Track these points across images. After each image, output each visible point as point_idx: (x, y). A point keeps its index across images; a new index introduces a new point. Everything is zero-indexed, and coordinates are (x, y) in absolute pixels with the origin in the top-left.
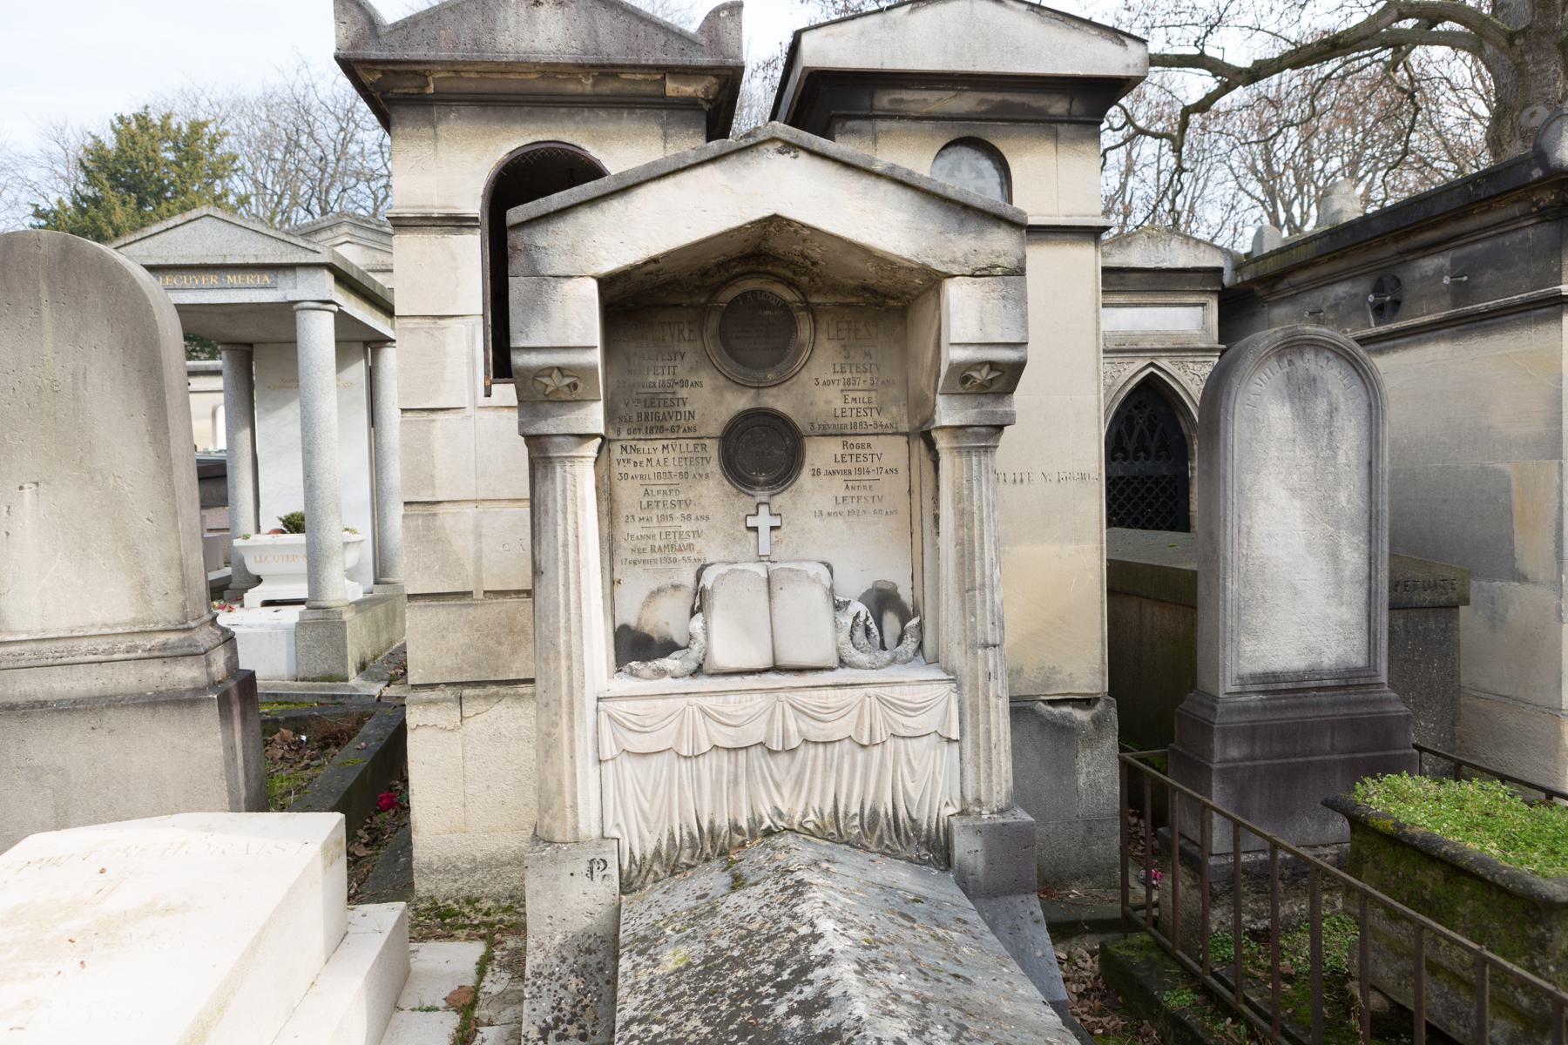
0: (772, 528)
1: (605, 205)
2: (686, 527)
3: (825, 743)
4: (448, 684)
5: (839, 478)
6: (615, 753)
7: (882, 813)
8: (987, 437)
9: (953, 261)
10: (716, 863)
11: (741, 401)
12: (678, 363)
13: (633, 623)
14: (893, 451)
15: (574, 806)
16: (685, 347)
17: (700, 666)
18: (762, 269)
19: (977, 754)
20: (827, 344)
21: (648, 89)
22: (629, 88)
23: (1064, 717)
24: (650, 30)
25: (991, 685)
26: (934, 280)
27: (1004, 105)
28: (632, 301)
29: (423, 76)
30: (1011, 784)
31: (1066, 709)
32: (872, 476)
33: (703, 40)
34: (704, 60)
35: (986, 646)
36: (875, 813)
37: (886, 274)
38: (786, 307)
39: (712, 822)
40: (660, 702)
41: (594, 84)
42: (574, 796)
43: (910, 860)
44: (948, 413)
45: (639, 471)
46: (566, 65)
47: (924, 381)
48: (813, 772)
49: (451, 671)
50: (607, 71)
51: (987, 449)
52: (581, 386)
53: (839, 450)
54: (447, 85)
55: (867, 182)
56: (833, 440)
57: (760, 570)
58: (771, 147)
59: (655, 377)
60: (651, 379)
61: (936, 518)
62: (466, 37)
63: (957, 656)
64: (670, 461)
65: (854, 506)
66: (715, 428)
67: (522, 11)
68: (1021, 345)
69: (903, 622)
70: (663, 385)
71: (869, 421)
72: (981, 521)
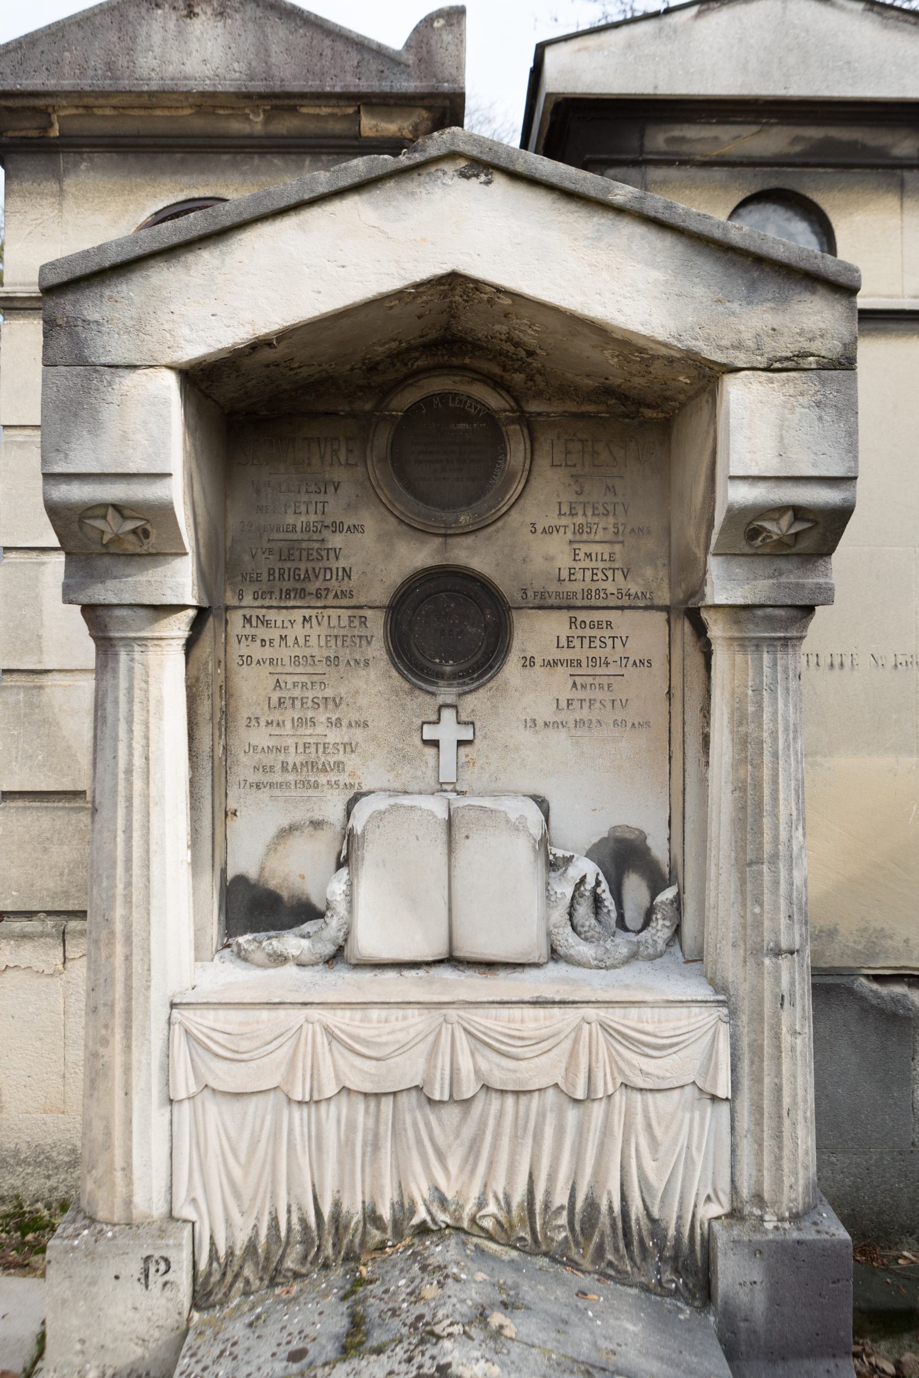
0: (460, 743)
1: (190, 258)
2: (334, 736)
3: (517, 1093)
4: (49, 913)
5: (562, 672)
6: (193, 1089)
7: (604, 1208)
8: (786, 624)
9: (738, 347)
10: (337, 1273)
11: (419, 555)
12: (330, 497)
13: (252, 873)
14: (646, 634)
15: (128, 1169)
16: (340, 474)
17: (341, 949)
18: (455, 361)
19: (759, 1123)
20: (550, 473)
21: (338, 127)
22: (312, 127)
23: (896, 1000)
24: (340, 46)
25: (785, 1016)
26: (707, 376)
27: (827, 145)
28: (249, 405)
29: (45, 113)
30: (813, 1169)
31: (899, 989)
32: (611, 670)
33: (410, 59)
34: (409, 85)
35: (777, 953)
36: (592, 1205)
37: (635, 368)
38: (489, 417)
39: (337, 1204)
40: (265, 1014)
41: (268, 121)
42: (128, 1154)
43: (645, 1288)
44: (725, 585)
45: (268, 653)
46: (226, 94)
47: (691, 532)
48: (497, 1136)
49: (54, 896)
50: (281, 102)
51: (785, 642)
52: (153, 532)
53: (564, 630)
54: (76, 126)
55: (601, 221)
56: (555, 615)
57: (436, 807)
58: (449, 168)
59: (297, 518)
60: (290, 519)
61: (706, 740)
62: (97, 61)
63: (730, 963)
64: (313, 641)
65: (584, 714)
66: (381, 594)
67: (171, 25)
68: (849, 480)
69: (655, 890)
70: (306, 529)
71: (610, 587)
72: (775, 755)
